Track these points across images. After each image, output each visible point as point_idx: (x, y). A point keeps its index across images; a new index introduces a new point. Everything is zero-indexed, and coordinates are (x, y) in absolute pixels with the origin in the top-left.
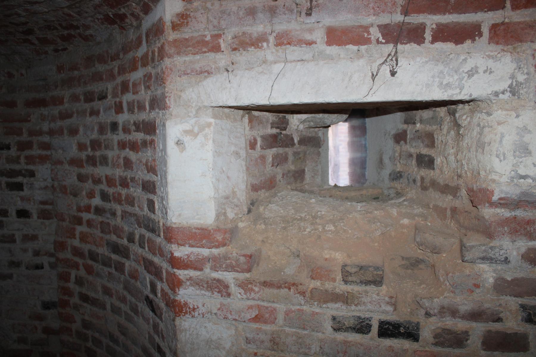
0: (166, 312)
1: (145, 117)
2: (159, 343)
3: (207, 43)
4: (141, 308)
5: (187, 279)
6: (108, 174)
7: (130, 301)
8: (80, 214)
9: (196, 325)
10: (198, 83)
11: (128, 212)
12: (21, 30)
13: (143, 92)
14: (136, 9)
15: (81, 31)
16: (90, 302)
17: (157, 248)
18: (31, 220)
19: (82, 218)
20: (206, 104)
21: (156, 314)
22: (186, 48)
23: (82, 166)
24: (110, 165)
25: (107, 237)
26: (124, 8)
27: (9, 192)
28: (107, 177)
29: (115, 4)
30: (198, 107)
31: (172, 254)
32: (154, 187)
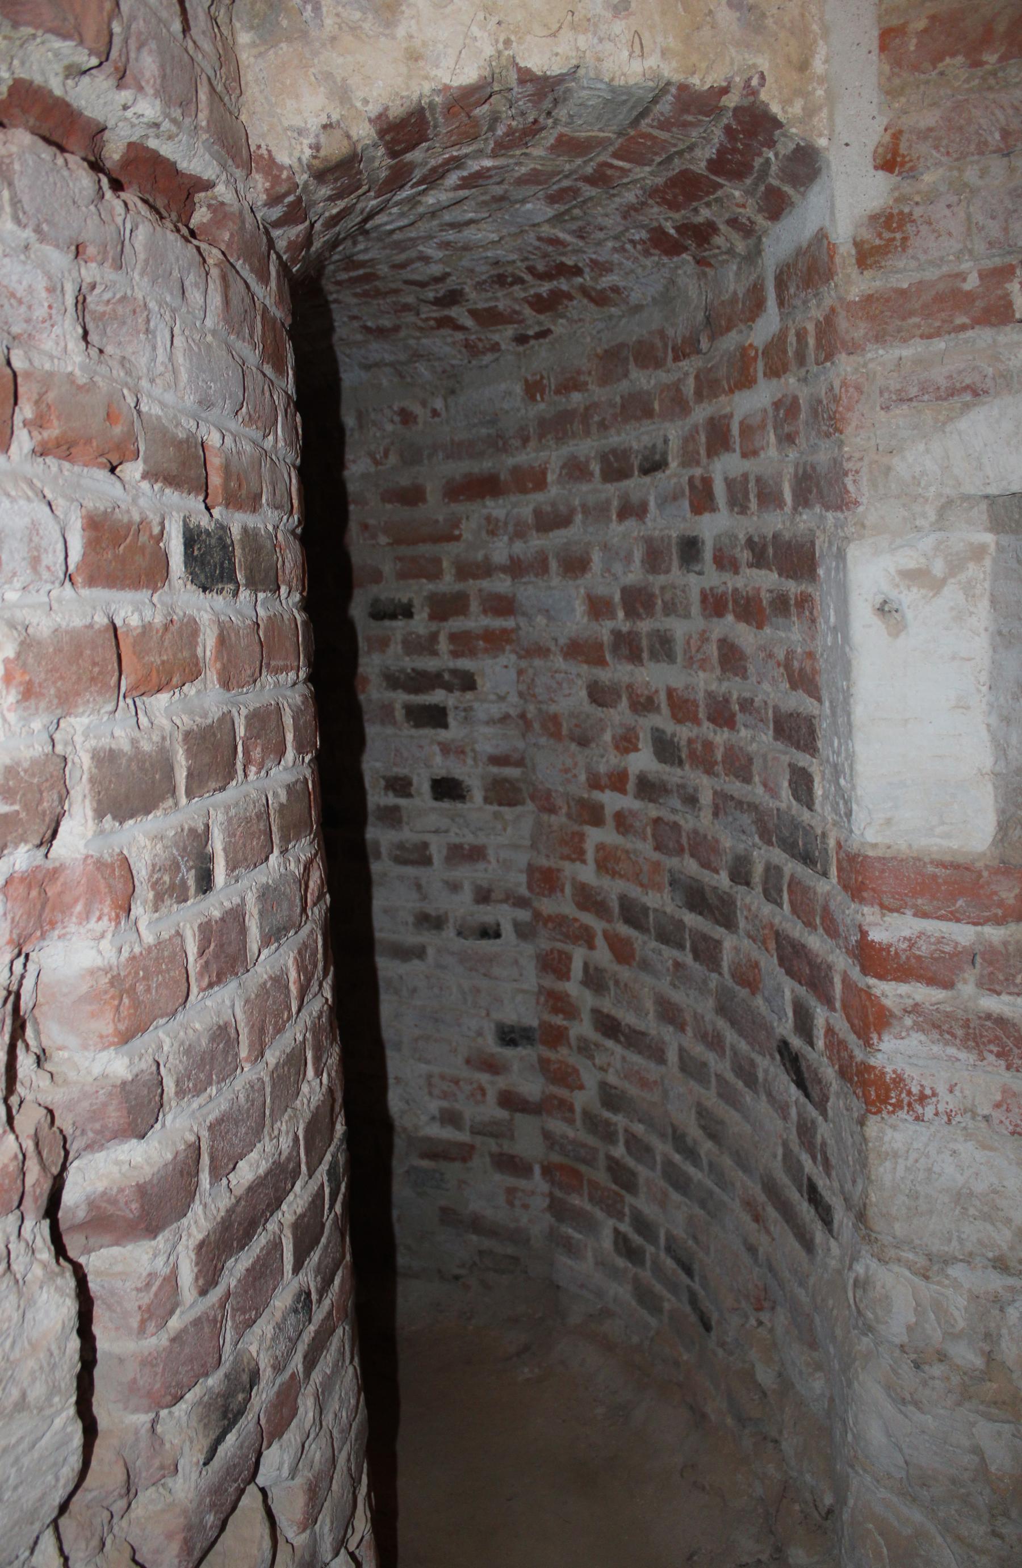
0: (838, 1095)
1: (780, 526)
2: (815, 1178)
3: (970, 297)
4: (766, 1071)
5: (905, 1011)
6: (674, 685)
7: (733, 1047)
8: (597, 795)
9: (926, 1145)
10: (944, 424)
11: (732, 798)
12: (431, 295)
13: (772, 452)
14: (744, 206)
15: (586, 279)
16: (622, 1039)
17: (819, 909)
18: (468, 805)
19: (602, 807)
20: (969, 489)
21: (807, 1095)
22: (904, 319)
23: (602, 662)
24: (679, 660)
25: (672, 862)
26: (708, 205)
27: (413, 732)
28: (670, 693)
29: (681, 198)
30: (943, 500)
31: (864, 934)
32: (812, 732)
